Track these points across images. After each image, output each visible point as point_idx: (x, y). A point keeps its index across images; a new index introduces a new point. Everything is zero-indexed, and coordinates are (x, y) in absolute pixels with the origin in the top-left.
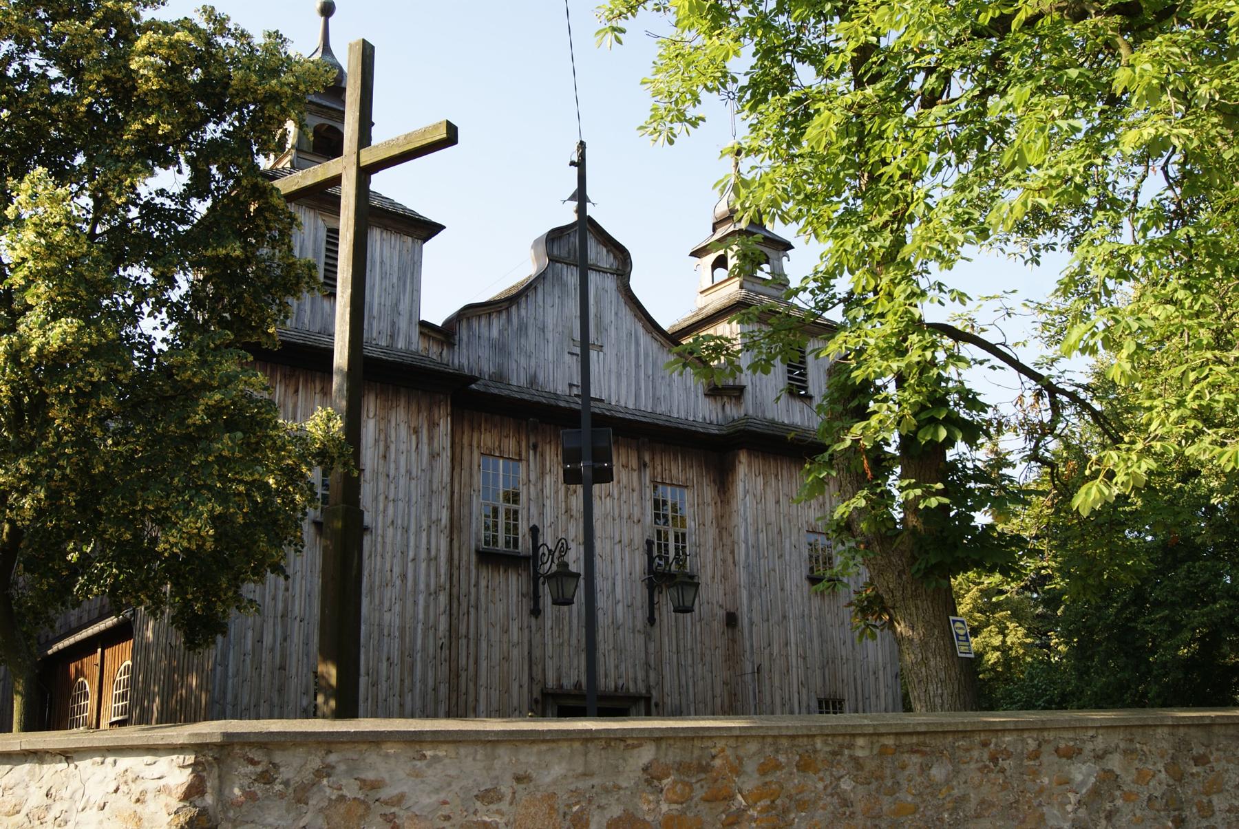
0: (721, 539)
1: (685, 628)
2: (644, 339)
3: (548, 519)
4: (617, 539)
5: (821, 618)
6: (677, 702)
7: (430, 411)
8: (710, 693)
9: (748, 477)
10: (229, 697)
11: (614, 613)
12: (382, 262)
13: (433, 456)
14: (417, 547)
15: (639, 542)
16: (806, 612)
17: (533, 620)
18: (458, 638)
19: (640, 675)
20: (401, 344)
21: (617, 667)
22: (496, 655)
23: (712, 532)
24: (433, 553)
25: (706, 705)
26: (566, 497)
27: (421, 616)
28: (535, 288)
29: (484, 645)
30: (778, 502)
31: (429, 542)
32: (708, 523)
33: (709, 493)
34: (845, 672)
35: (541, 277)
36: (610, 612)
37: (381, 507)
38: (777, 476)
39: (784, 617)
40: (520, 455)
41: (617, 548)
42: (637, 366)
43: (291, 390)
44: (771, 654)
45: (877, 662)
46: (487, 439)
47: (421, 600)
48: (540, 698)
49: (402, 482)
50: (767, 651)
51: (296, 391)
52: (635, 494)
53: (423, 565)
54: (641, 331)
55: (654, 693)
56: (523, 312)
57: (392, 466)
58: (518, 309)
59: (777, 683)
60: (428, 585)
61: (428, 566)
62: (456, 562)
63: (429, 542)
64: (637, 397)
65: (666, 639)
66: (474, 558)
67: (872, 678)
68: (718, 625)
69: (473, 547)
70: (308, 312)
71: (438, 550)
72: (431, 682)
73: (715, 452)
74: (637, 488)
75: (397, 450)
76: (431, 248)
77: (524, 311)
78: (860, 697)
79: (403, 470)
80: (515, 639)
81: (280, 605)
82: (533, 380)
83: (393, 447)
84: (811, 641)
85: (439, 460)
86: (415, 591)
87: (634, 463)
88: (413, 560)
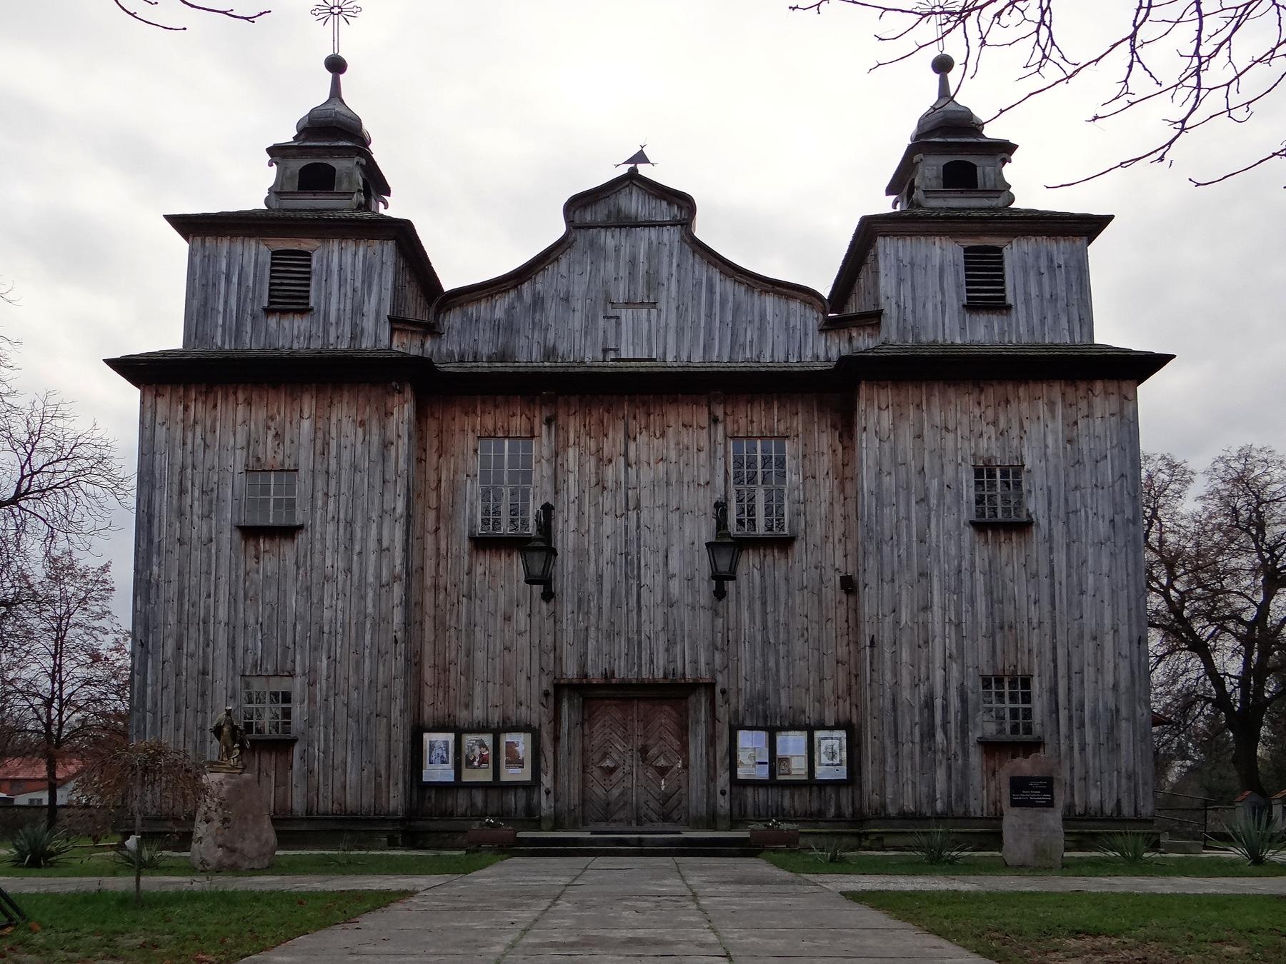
0: (843, 491)
1: (776, 598)
2: (723, 286)
5: (990, 573)
9: (876, 413)
10: (149, 705)
11: (666, 588)
12: (340, 271)
13: (386, 445)
15: (704, 501)
16: (965, 564)
17: (544, 605)
20: (367, 343)
23: (826, 488)
24: (385, 544)
26: (598, 467)
28: (557, 259)
30: (919, 436)
31: (380, 534)
32: (821, 474)
33: (825, 440)
34: (1035, 640)
37: (320, 503)
38: (919, 406)
39: (922, 574)
43: (210, 405)
44: (897, 622)
45: (1100, 625)
48: (551, 690)
49: (345, 476)
50: (889, 620)
51: (215, 406)
53: (373, 557)
54: (717, 277)
55: (719, 678)
56: (539, 287)
57: (333, 462)
59: (905, 656)
60: (378, 576)
61: (379, 559)
62: (443, 552)
63: (380, 534)
65: (745, 615)
66: (466, 545)
67: (1089, 646)
68: (832, 591)
70: (249, 330)
73: (830, 394)
74: (706, 449)
75: (339, 445)
76: (1098, 251)
77: (541, 283)
78: (1062, 670)
79: (346, 464)
83: (333, 444)
84: (972, 601)
87: (703, 418)
88: (360, 553)
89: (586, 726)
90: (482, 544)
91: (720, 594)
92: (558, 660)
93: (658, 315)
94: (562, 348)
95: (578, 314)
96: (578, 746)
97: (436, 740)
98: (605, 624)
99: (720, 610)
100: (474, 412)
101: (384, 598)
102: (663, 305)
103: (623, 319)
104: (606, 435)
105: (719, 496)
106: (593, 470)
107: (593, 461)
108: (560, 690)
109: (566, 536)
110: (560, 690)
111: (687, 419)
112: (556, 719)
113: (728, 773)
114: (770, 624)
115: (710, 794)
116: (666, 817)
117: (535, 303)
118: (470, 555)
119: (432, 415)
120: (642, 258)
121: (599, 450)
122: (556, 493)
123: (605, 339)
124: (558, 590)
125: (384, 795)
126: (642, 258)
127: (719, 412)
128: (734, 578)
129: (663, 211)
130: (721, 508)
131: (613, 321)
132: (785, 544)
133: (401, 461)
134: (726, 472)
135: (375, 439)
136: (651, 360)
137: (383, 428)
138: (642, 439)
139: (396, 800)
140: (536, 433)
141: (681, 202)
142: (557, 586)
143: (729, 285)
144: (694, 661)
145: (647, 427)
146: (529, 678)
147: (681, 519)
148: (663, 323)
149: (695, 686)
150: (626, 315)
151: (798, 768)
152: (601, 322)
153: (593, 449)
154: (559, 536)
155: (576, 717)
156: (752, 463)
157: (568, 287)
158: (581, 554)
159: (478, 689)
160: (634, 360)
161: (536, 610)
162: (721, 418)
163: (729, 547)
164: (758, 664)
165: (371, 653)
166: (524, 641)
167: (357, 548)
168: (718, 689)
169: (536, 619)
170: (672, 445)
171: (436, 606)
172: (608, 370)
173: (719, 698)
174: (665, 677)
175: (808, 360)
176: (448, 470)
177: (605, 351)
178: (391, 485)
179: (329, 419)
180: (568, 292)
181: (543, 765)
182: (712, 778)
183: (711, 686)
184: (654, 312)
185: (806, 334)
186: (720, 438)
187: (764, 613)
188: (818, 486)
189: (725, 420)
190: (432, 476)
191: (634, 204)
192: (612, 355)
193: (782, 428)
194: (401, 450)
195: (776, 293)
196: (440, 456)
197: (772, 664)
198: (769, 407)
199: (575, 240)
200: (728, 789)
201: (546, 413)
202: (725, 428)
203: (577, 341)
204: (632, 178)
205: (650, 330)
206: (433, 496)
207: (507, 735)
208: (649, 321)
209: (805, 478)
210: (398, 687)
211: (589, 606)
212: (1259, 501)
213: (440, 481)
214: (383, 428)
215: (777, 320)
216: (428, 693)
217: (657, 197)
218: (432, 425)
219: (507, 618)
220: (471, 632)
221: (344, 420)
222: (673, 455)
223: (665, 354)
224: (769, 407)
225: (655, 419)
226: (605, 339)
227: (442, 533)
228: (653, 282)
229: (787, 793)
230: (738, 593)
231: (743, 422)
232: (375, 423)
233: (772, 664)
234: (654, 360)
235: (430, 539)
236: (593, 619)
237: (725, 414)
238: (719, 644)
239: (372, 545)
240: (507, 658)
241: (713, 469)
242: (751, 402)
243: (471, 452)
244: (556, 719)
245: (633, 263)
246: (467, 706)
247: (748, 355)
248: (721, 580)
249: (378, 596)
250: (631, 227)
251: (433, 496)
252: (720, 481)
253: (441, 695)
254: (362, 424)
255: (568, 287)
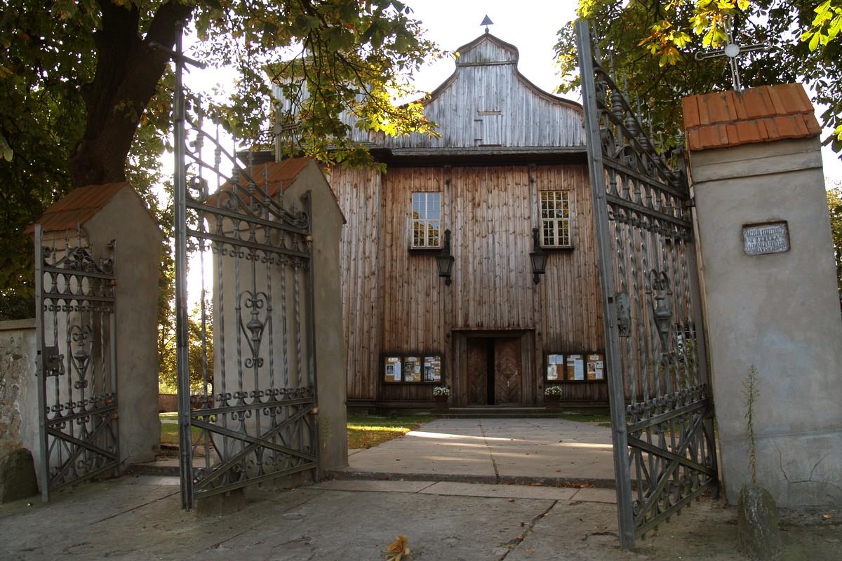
2: (533, 101)
3: (460, 223)
4: (511, 231)
6: (558, 331)
7: (529, 172)
8: (585, 324)
13: (367, 198)
14: (357, 252)
15: (526, 228)
18: (396, 302)
19: (529, 315)
21: (509, 312)
22: (421, 310)
24: (367, 254)
25: (583, 332)
26: (473, 209)
27: (359, 291)
28: (451, 86)
29: (413, 305)
35: (454, 77)
36: (505, 278)
40: (439, 188)
41: (512, 237)
42: (527, 119)
46: (416, 182)
47: (360, 281)
48: (451, 334)
52: (526, 201)
54: (531, 96)
55: (538, 327)
56: (442, 102)
58: (439, 101)
60: (364, 273)
62: (395, 258)
64: (498, 141)
65: (550, 292)
66: (406, 254)
69: (406, 248)
71: (371, 252)
72: (366, 328)
80: (435, 299)
81: (405, 307)
82: (448, 142)
85: (371, 200)
86: (356, 277)
87: (525, 179)
88: (355, 259)
89: (469, 352)
90: (414, 253)
91: (536, 281)
92: (455, 317)
93: (502, 119)
94: (454, 139)
95: (461, 118)
96: (465, 365)
97: (395, 361)
98: (477, 298)
99: (537, 290)
100: (410, 177)
101: (366, 284)
102: (504, 113)
103: (484, 121)
104: (477, 190)
105: (534, 226)
106: (470, 211)
107: (470, 204)
108: (455, 335)
109: (457, 251)
110: (455, 335)
111: (518, 180)
112: (453, 350)
113: (542, 378)
114: (563, 297)
115: (534, 389)
116: (510, 401)
117: (439, 111)
118: (408, 259)
119: (389, 180)
120: (493, 84)
121: (473, 199)
122: (452, 224)
123: (476, 134)
124: (454, 279)
125: (367, 389)
126: (493, 84)
127: (534, 176)
128: (544, 273)
129: (503, 56)
130: (536, 231)
131: (479, 122)
132: (569, 251)
133: (375, 207)
134: (538, 210)
135: (362, 195)
136: (498, 145)
137: (366, 188)
138: (495, 192)
139: (372, 390)
140: (441, 189)
141: (512, 50)
142: (453, 277)
143: (537, 100)
144: (524, 318)
145: (498, 186)
146: (439, 327)
147: (516, 237)
148: (504, 124)
149: (525, 331)
150: (486, 119)
151: (578, 375)
152: (473, 123)
153: (470, 199)
154: (454, 249)
155: (464, 347)
156: (551, 205)
157: (456, 102)
158: (465, 260)
159: (413, 333)
160: (490, 145)
161: (442, 290)
162: (535, 180)
163: (542, 253)
164: (558, 319)
165: (360, 314)
166: (435, 307)
167: (353, 257)
168: (537, 332)
169: (442, 295)
170: (510, 196)
171: (391, 288)
172: (478, 153)
173: (537, 338)
174: (509, 326)
175: (578, 145)
176: (397, 211)
177: (476, 140)
178: (369, 221)
179: (339, 183)
180: (456, 105)
181: (447, 374)
182: (534, 380)
183: (534, 331)
184: (500, 116)
185: (576, 129)
186: (534, 191)
187: (559, 291)
188: (585, 218)
189: (537, 181)
190: (389, 214)
191: (489, 52)
192: (479, 143)
193: (566, 185)
194: (376, 199)
195: (560, 104)
196: (393, 203)
197: (564, 319)
198: (559, 173)
199: (459, 74)
200: (542, 385)
201: (447, 178)
202: (537, 185)
203: (463, 134)
204: (487, 36)
205: (498, 128)
206: (389, 226)
207: (399, 363)
208: (497, 122)
209: (579, 214)
210: (373, 332)
211: (469, 288)
212: (116, 404)
213: (393, 218)
214: (366, 188)
215: (561, 121)
216: (387, 334)
217: (499, 47)
218: (389, 185)
219: (428, 295)
220: (409, 303)
221: (347, 184)
222: (511, 202)
223: (506, 142)
224: (559, 173)
225: (501, 181)
226: (476, 134)
227: (394, 247)
228: (501, 100)
229: (573, 387)
230: (546, 280)
231: (546, 182)
232: (362, 185)
233: (564, 319)
234: (501, 145)
235: (388, 250)
236: (471, 295)
237: (537, 177)
238: (537, 308)
239: (360, 255)
240: (428, 316)
241: (531, 209)
242: (550, 170)
243: (409, 201)
244: (453, 350)
245: (488, 87)
246: (407, 343)
247: (548, 142)
248: (537, 274)
249: (363, 283)
250: (487, 65)
251: (389, 226)
252: (534, 217)
253: (394, 336)
254: (356, 186)
255: (456, 102)
